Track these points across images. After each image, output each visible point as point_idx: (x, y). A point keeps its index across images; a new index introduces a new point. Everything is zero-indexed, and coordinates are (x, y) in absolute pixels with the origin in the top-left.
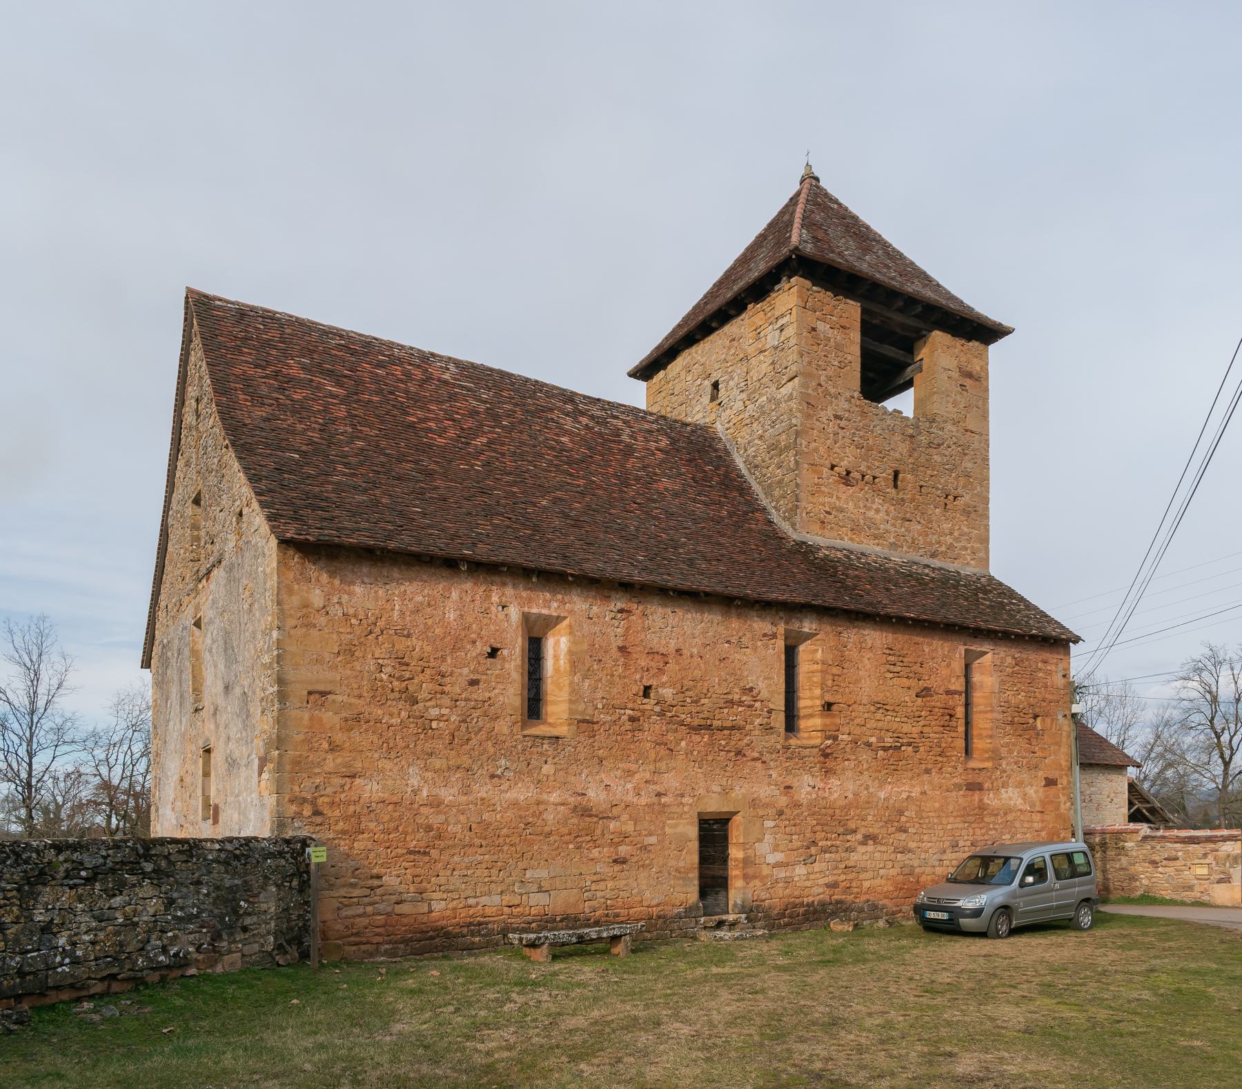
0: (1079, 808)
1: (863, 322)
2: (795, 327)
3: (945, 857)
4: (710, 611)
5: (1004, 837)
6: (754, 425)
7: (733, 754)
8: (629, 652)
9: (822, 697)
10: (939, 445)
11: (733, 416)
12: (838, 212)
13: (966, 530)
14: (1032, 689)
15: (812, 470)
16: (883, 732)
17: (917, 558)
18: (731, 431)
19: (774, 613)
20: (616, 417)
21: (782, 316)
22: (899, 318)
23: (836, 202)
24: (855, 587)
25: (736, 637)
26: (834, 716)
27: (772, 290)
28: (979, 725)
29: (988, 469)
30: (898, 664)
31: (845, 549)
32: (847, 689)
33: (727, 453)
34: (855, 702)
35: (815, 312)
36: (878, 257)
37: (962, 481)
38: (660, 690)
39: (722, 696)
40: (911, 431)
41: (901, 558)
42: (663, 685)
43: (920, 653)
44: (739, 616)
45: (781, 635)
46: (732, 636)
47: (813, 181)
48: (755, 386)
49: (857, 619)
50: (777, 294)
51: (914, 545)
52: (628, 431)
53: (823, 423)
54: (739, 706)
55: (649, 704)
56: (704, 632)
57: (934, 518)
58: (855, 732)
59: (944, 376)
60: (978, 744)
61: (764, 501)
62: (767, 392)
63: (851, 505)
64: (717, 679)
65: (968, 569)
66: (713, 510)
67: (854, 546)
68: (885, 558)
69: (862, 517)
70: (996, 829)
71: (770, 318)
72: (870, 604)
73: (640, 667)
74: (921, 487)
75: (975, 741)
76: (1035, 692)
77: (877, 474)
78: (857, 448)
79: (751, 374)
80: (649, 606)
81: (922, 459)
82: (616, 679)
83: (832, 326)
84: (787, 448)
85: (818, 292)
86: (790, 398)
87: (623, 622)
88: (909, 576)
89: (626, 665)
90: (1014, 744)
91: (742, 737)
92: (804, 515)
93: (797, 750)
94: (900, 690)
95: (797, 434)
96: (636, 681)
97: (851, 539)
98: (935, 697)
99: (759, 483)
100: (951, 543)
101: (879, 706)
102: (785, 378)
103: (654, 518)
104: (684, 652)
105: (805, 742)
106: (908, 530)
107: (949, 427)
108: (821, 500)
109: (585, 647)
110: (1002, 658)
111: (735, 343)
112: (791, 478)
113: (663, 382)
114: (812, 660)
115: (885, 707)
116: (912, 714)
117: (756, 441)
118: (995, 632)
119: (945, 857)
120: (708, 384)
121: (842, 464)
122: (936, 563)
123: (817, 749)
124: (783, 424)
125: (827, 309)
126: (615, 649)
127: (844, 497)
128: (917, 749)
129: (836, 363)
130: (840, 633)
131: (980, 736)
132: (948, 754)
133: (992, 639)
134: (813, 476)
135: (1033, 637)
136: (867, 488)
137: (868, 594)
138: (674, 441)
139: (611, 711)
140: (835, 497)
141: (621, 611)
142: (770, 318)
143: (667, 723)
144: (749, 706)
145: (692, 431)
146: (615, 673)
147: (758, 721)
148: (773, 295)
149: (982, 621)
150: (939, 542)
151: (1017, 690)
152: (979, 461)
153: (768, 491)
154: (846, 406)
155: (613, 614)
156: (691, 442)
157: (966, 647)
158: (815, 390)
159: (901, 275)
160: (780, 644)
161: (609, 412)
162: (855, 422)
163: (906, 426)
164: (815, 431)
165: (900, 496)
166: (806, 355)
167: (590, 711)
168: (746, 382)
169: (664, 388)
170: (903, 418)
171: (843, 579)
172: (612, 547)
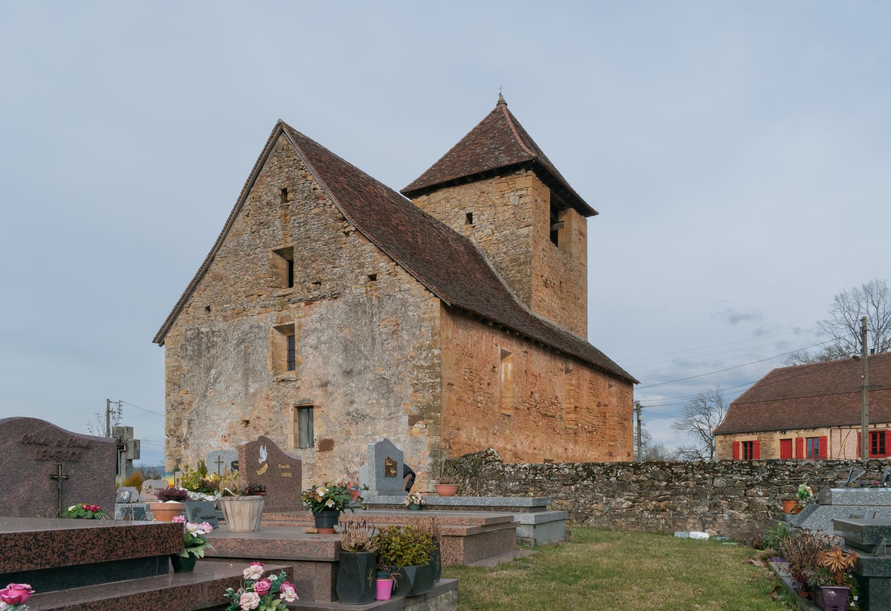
21: (521, 189)
50: (515, 176)
86: (527, 236)
97: (547, 317)
99: (504, 278)
102: (524, 224)
113: (426, 203)
120: (463, 213)
169: (427, 206)
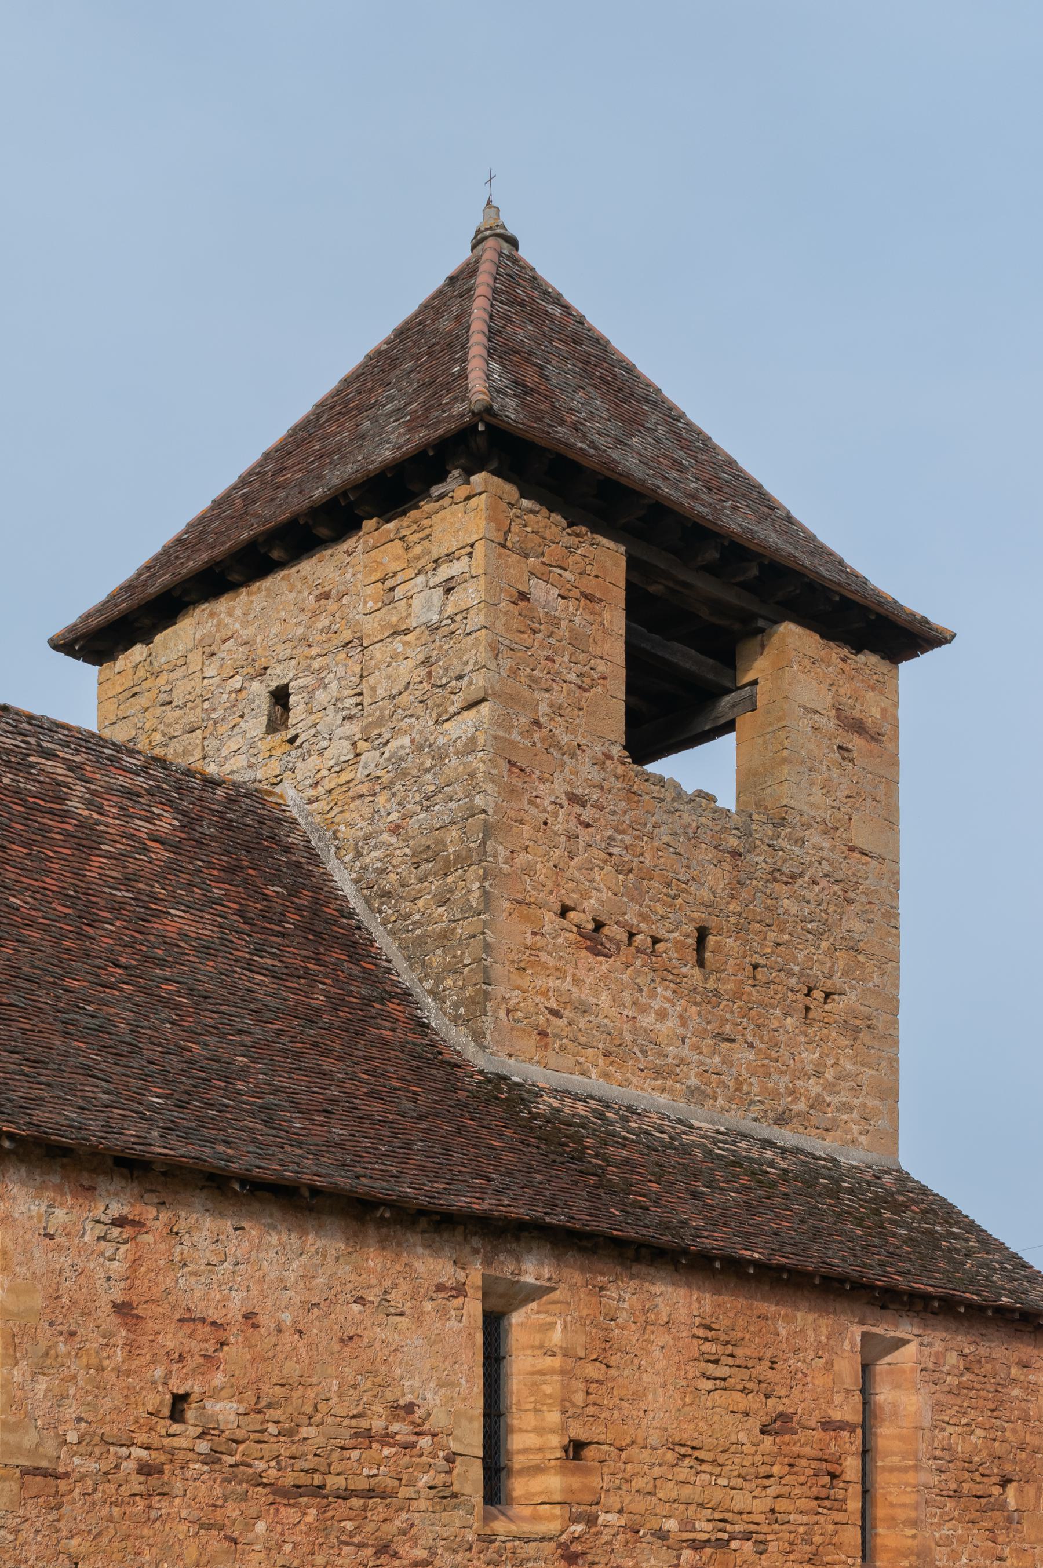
1: (631, 587)
2: (482, 587)
4: (319, 1229)
6: (381, 799)
7: (371, 1551)
8: (138, 1317)
9: (564, 1428)
10: (793, 877)
11: (325, 773)
12: (563, 327)
13: (849, 1067)
14: (998, 1422)
15: (521, 916)
16: (693, 1508)
17: (746, 1125)
18: (322, 805)
19: (460, 1238)
20: (50, 755)
22: (706, 586)
23: (557, 300)
24: (628, 1187)
25: (379, 1291)
26: (587, 1471)
27: (424, 493)
28: (890, 1498)
29: (898, 936)
30: (725, 1360)
31: (592, 1097)
32: (616, 1414)
33: (314, 858)
34: (633, 1442)
35: (526, 556)
36: (658, 441)
37: (842, 958)
38: (208, 1404)
39: (346, 1422)
40: (734, 842)
41: (713, 1123)
42: (215, 1394)
43: (770, 1337)
44: (383, 1243)
45: (476, 1288)
46: (369, 1287)
47: (505, 245)
48: (382, 710)
49: (637, 1259)
51: (739, 1094)
52: (80, 788)
53: (545, 811)
54: (384, 1444)
55: (185, 1434)
56: (307, 1278)
57: (783, 1038)
58: (633, 1507)
59: (804, 725)
60: (886, 1537)
61: (407, 977)
62: (411, 727)
63: (604, 999)
64: (335, 1382)
65: (854, 1153)
66: (294, 991)
67: (612, 1091)
68: (680, 1121)
69: (627, 1026)
71: (418, 558)
72: (667, 1227)
73: (163, 1351)
74: (755, 967)
75: (880, 1530)
76: (1004, 1430)
77: (662, 933)
78: (618, 872)
79: (372, 680)
80: (183, 1214)
81: (758, 906)
82: (110, 1377)
83: (563, 592)
84: (463, 860)
85: (531, 511)
86: (470, 747)
87: (123, 1248)
88: (734, 1164)
89: (132, 1348)
90: (961, 1541)
91: (391, 1512)
92: (502, 1014)
93: (509, 1545)
94: (729, 1418)
95: (488, 830)
96: (153, 1382)
97: (606, 1075)
98: (801, 1435)
99: (392, 933)
100: (819, 1095)
101: (683, 1450)
102: (459, 701)
103: (167, 1003)
104: (262, 1319)
105: (527, 1528)
106: (726, 1061)
107: (814, 838)
108: (539, 983)
109: (38, 1301)
110: (937, 1355)
111: (331, 605)
112: (472, 930)
113: (141, 673)
114: (541, 1347)
115: (696, 1453)
116: (753, 1470)
117: (385, 837)
118: (926, 1298)
120: (259, 691)
121: (585, 904)
122: (786, 1137)
123: (553, 1544)
124: (453, 805)
125: (553, 553)
126: (109, 1309)
127: (589, 979)
128: (762, 1547)
129: (573, 677)
130: (602, 1289)
131: (892, 1522)
132: (827, 1559)
133: (918, 1312)
134: (523, 927)
135: (1000, 1310)
136: (638, 963)
137: (657, 1203)
138: (189, 822)
139: (97, 1451)
140: (569, 978)
141: (120, 1222)
142: (418, 558)
143: (224, 1480)
144: (407, 1446)
145: (230, 799)
146: (106, 1363)
147: (425, 1479)
148: (427, 507)
149: (896, 1273)
150: (792, 1092)
151: (967, 1425)
152: (878, 918)
153: (416, 955)
154: (595, 775)
155: (100, 1230)
156: (228, 826)
157: (865, 1328)
158: (526, 733)
159: (709, 489)
160: (474, 1308)
161: (32, 740)
162: (614, 812)
163: (725, 829)
164: (526, 828)
165: (711, 985)
166: (506, 653)
167: (50, 1448)
168: (359, 699)
169: (145, 685)
170: (716, 810)
171: (600, 1167)
172: (87, 1071)
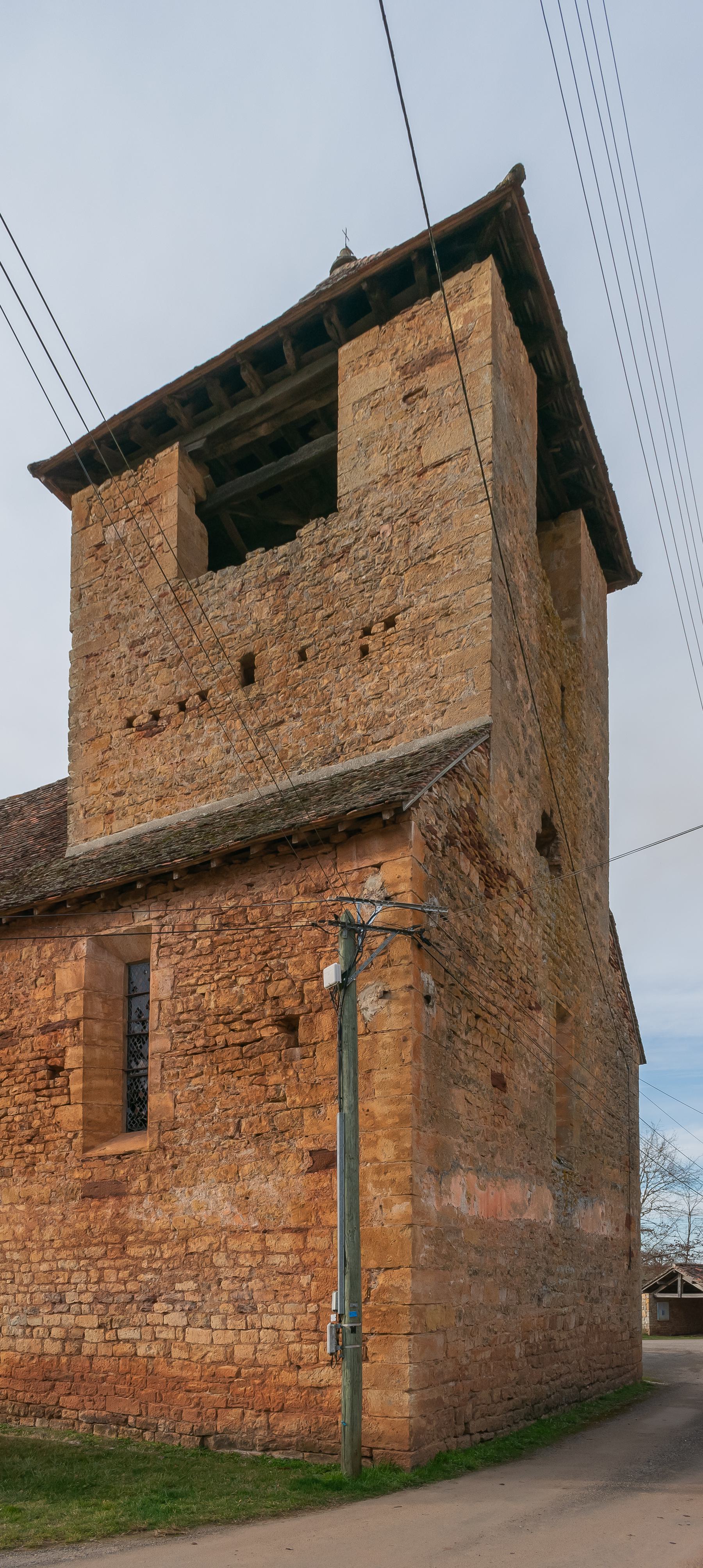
0: (474, 746)
3: (35, 1321)
5: (178, 1287)
70: (158, 1271)
119: (35, 1321)
